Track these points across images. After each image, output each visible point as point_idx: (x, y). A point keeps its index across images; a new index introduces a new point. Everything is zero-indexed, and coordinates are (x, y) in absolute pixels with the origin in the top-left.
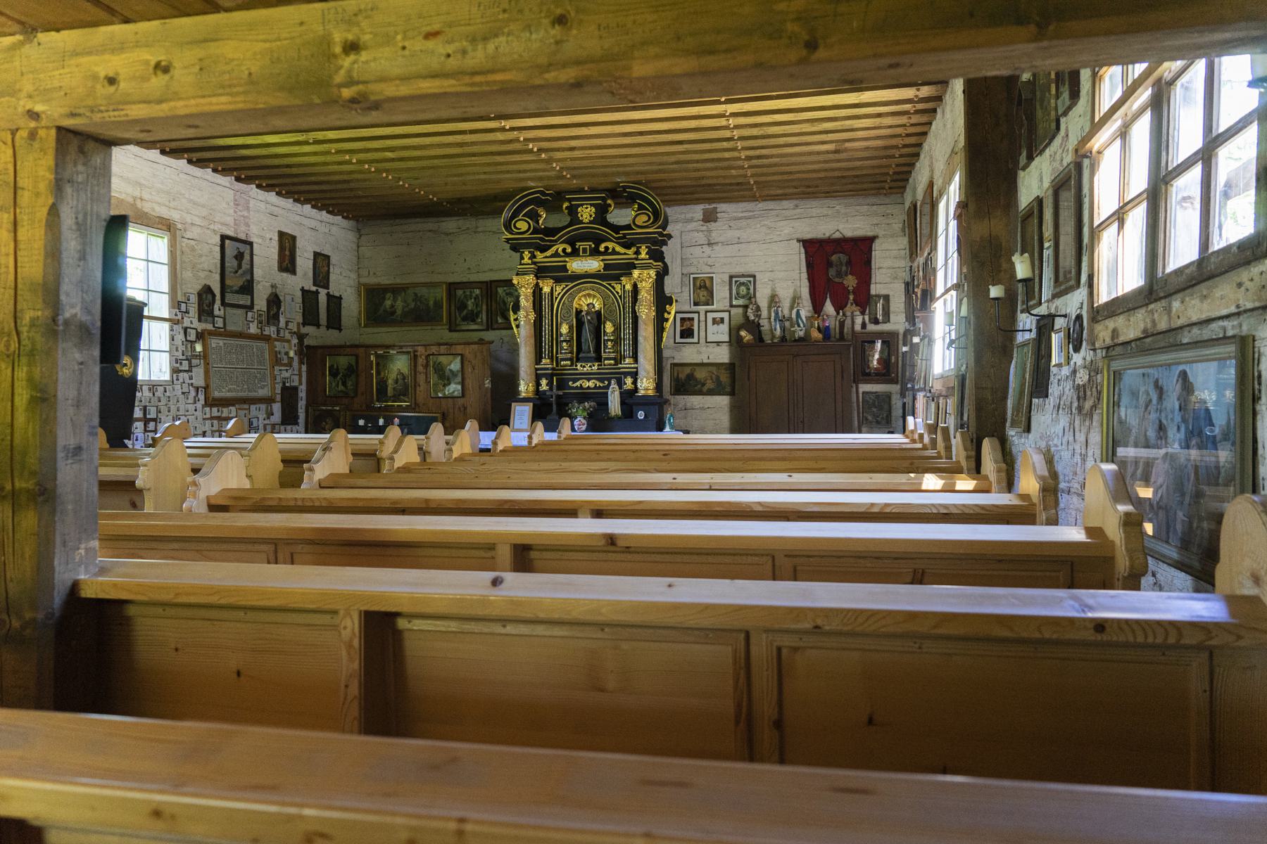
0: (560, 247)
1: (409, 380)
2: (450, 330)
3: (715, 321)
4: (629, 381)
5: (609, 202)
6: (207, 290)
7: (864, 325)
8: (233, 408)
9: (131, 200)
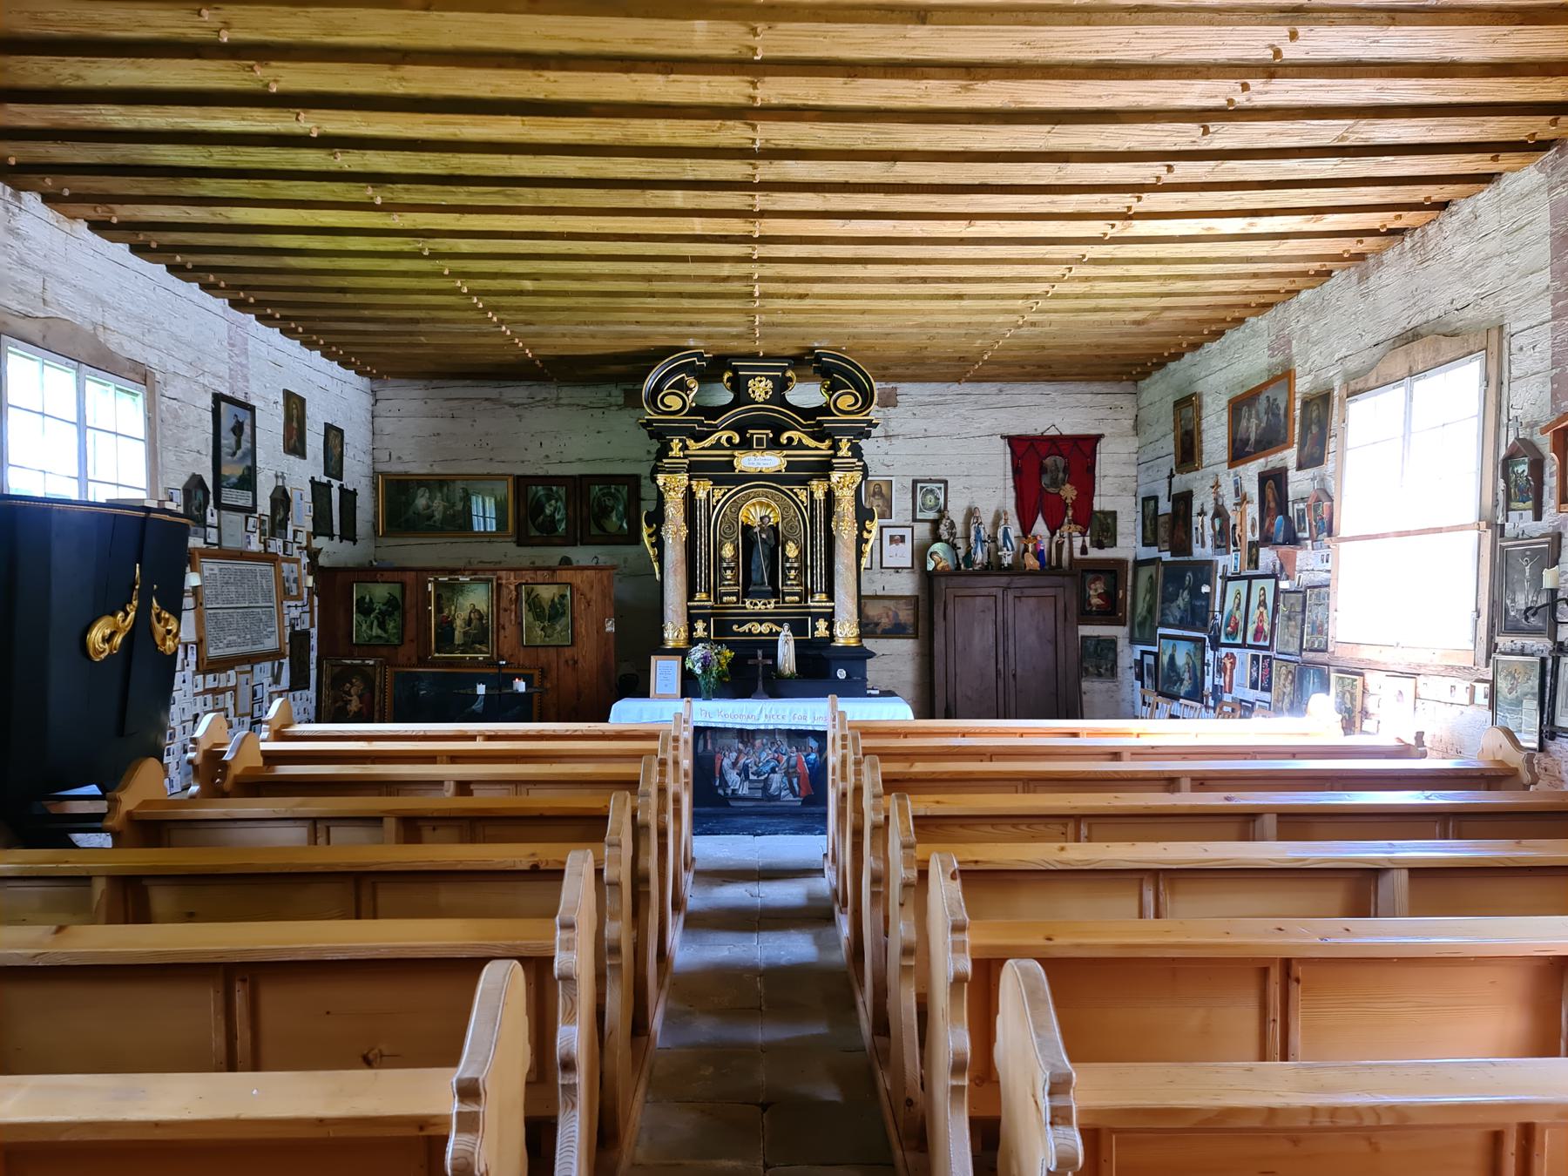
0: (725, 435)
1: (491, 623)
2: (519, 544)
3: (892, 539)
4: (822, 624)
5: (789, 374)
6: (196, 482)
7: (1084, 550)
8: (232, 673)
9: (89, 328)
